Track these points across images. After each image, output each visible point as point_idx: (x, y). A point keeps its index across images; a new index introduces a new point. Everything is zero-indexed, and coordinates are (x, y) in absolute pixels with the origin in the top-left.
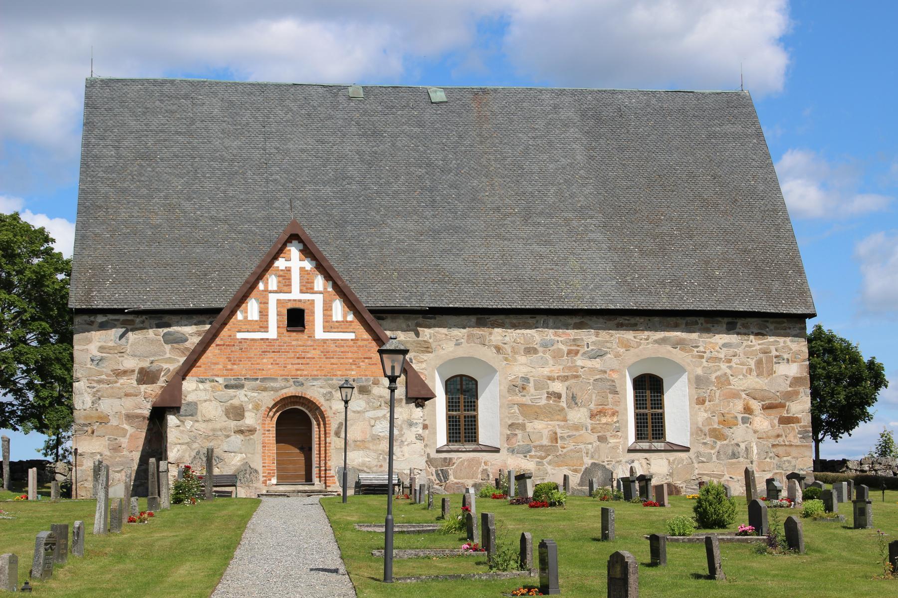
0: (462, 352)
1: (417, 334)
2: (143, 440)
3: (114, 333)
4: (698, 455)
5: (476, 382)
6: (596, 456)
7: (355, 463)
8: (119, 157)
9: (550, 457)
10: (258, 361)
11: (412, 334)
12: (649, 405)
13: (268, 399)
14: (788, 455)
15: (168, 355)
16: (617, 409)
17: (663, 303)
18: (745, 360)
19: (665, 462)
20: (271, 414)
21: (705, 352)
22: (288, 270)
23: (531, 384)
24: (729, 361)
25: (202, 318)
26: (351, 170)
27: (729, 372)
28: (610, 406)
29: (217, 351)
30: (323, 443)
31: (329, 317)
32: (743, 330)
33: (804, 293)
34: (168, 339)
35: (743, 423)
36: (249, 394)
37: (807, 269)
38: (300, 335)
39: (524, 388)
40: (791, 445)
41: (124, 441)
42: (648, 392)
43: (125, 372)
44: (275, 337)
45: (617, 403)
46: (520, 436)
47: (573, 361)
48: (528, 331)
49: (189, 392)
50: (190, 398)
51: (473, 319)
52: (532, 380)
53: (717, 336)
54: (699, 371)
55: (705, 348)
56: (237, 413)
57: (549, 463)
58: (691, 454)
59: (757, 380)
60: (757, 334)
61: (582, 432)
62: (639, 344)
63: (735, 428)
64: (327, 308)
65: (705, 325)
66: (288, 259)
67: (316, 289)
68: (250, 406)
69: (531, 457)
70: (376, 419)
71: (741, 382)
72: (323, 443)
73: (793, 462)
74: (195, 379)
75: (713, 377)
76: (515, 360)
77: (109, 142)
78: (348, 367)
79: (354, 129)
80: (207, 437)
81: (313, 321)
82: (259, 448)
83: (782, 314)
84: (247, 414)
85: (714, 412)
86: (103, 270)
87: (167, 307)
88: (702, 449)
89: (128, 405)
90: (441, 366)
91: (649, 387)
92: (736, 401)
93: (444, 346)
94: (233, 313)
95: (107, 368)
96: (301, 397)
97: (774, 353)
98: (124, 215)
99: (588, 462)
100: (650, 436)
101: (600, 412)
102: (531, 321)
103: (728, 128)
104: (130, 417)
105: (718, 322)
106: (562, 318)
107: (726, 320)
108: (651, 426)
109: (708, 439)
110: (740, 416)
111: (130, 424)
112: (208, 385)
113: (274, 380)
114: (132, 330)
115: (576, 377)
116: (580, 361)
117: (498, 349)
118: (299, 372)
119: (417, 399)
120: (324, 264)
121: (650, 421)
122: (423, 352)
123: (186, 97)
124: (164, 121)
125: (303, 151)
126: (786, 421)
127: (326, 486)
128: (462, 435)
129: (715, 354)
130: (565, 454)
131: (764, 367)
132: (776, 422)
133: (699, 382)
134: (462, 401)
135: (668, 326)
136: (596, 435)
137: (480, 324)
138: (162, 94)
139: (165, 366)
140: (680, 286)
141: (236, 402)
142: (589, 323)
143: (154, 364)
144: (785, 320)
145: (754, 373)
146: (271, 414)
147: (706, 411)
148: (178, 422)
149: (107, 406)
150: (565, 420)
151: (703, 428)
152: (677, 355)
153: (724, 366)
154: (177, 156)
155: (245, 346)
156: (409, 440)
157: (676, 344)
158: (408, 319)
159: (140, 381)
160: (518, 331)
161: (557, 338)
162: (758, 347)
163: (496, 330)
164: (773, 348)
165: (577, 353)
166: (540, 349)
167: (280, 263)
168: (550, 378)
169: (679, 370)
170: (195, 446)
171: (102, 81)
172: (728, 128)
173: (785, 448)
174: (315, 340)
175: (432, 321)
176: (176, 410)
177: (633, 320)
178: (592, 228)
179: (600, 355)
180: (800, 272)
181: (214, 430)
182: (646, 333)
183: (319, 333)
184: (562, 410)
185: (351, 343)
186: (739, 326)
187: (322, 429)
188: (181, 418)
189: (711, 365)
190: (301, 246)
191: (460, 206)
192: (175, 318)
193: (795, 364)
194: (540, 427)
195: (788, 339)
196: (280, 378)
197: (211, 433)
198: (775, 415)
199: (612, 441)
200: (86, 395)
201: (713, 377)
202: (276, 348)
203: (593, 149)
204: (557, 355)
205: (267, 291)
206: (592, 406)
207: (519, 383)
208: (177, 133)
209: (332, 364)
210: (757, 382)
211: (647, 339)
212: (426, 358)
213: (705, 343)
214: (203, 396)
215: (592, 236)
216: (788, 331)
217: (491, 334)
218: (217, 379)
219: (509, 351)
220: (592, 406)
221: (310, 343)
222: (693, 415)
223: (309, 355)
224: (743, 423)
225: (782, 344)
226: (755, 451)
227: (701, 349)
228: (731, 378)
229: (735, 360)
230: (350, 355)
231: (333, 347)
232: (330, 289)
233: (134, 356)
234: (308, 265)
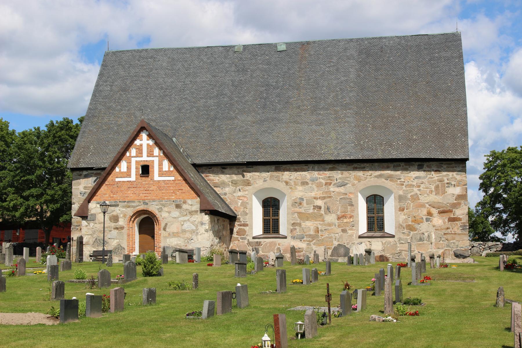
0: (267, 185)
1: (243, 176)
4: (400, 239)
5: (383, 198)
6: (341, 240)
7: (173, 244)
8: (111, 90)
9: (314, 241)
11: (241, 176)
16: (353, 214)
17: (379, 155)
18: (429, 186)
19: (380, 243)
20: (133, 219)
21: (404, 182)
22: (141, 145)
23: (305, 202)
24: (419, 186)
26: (226, 91)
27: (419, 193)
29: (106, 188)
31: (161, 168)
32: (427, 169)
33: (465, 146)
35: (427, 221)
36: (121, 209)
39: (300, 204)
40: (455, 234)
44: (134, 180)
45: (353, 211)
46: (298, 230)
48: (304, 173)
49: (92, 209)
51: (273, 167)
52: (305, 199)
53: (412, 173)
54: (401, 193)
55: (404, 179)
57: (314, 244)
58: (396, 239)
59: (436, 197)
60: (436, 171)
61: (333, 227)
62: (366, 178)
63: (421, 224)
64: (161, 164)
65: (405, 167)
66: (141, 140)
67: (155, 155)
68: (122, 215)
69: (304, 241)
70: (184, 221)
71: (426, 198)
73: (457, 243)
75: (409, 196)
76: (296, 189)
77: (108, 83)
79: (233, 68)
82: (126, 237)
83: (431, 158)
84: (120, 219)
85: (409, 215)
86: (88, 148)
88: (402, 236)
90: (256, 192)
91: (375, 202)
92: (422, 209)
93: (258, 182)
94: (113, 168)
97: (446, 181)
98: (106, 120)
99: (336, 243)
101: (343, 216)
102: (305, 167)
105: (412, 165)
106: (323, 165)
107: (417, 163)
108: (376, 223)
109: (405, 230)
110: (424, 218)
113: (133, 202)
115: (330, 197)
116: (332, 188)
117: (287, 183)
118: (146, 198)
119: (205, 210)
122: (246, 185)
123: (151, 57)
125: (203, 82)
126: (452, 220)
128: (271, 229)
129: (410, 183)
130: (323, 239)
131: (440, 189)
132: (447, 220)
133: (401, 199)
134: (271, 211)
135: (383, 168)
136: (340, 229)
137: (277, 170)
138: (140, 57)
141: (114, 213)
142: (337, 167)
144: (453, 162)
145: (434, 193)
146: (133, 219)
147: (404, 215)
148: (87, 224)
150: (323, 221)
151: (403, 224)
152: (388, 184)
153: (416, 190)
154: (139, 88)
155: (119, 185)
156: (201, 232)
157: (388, 178)
158: (238, 168)
160: (298, 173)
161: (319, 176)
162: (436, 178)
163: (286, 173)
164: (445, 179)
165: (330, 184)
166: (310, 182)
167: (137, 142)
168: (315, 198)
169: (390, 192)
170: (95, 236)
173: (452, 235)
174: (154, 181)
175: (251, 169)
177: (362, 165)
178: (349, 115)
179: (343, 185)
182: (370, 172)
183: (156, 177)
184: (322, 215)
185: (172, 182)
186: (425, 166)
189: (408, 189)
191: (279, 107)
193: (459, 188)
194: (309, 224)
195: (455, 173)
196: (136, 201)
198: (446, 217)
201: (409, 196)
202: (135, 185)
204: (319, 185)
205: (131, 157)
206: (339, 213)
207: (298, 201)
208: (143, 76)
209: (163, 193)
210: (436, 198)
211: (371, 176)
212: (247, 189)
213: (405, 177)
215: (348, 119)
216: (455, 168)
217: (283, 175)
219: (293, 184)
221: (151, 182)
222: (396, 217)
223: (151, 189)
224: (427, 221)
225: (451, 176)
226: (434, 237)
227: (403, 180)
228: (420, 196)
229: (422, 186)
230: (172, 188)
232: (162, 154)
234: (151, 142)
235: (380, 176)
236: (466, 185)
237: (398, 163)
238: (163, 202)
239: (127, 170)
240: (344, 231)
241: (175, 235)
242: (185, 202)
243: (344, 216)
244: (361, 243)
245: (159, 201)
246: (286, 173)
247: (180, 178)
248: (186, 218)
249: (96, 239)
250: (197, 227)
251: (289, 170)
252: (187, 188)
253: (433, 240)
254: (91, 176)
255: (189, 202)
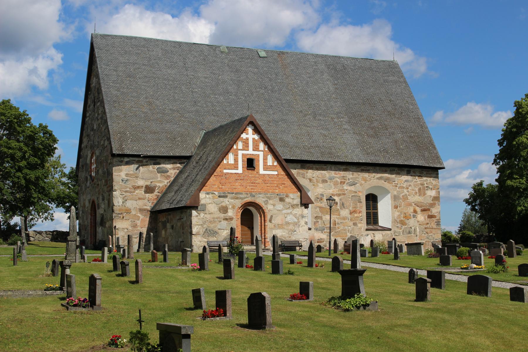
2: (148, 222)
3: (134, 167)
4: (395, 232)
10: (234, 184)
12: (371, 209)
13: (239, 203)
14: (431, 232)
15: (159, 179)
17: (382, 161)
18: (414, 188)
19: (381, 235)
22: (247, 139)
24: (408, 188)
25: (175, 161)
27: (407, 193)
28: (358, 209)
29: (215, 179)
30: (263, 225)
32: (413, 174)
33: (438, 158)
34: (160, 171)
36: (230, 200)
37: (437, 146)
38: (253, 172)
39: (321, 199)
41: (138, 223)
42: (371, 202)
43: (138, 187)
46: (320, 222)
47: (343, 187)
48: (323, 172)
49: (202, 199)
50: (202, 202)
51: (299, 165)
52: (325, 195)
53: (403, 177)
54: (395, 193)
56: (224, 210)
58: (392, 232)
60: (419, 176)
62: (371, 179)
64: (265, 159)
68: (230, 207)
69: (325, 232)
72: (263, 225)
74: (205, 192)
76: (318, 186)
78: (274, 188)
79: (227, 68)
80: (210, 222)
81: (259, 165)
84: (229, 210)
87: (160, 155)
89: (140, 203)
91: (372, 200)
92: (410, 207)
95: (130, 185)
96: (254, 203)
97: (426, 185)
100: (372, 223)
101: (354, 211)
102: (325, 167)
103: (391, 78)
104: (141, 210)
105: (403, 170)
106: (338, 166)
107: (406, 169)
108: (372, 218)
110: (412, 214)
111: (141, 214)
112: (211, 196)
113: (241, 194)
114: (142, 166)
115: (344, 194)
117: (310, 180)
118: (253, 190)
120: (265, 137)
121: (372, 216)
123: (144, 46)
124: (136, 58)
126: (431, 217)
127: (265, 247)
129: (402, 185)
131: (422, 192)
132: (426, 217)
133: (395, 198)
136: (352, 222)
137: (302, 168)
139: (158, 184)
140: (387, 152)
141: (224, 204)
143: (153, 183)
145: (418, 194)
147: (398, 212)
149: (130, 204)
150: (339, 215)
152: (386, 185)
153: (405, 191)
155: (227, 176)
157: (387, 180)
159: (146, 192)
161: (336, 176)
163: (309, 171)
164: (425, 183)
165: (344, 183)
166: (329, 181)
167: (244, 136)
170: (205, 226)
171: (100, 35)
172: (391, 78)
174: (260, 175)
176: (196, 208)
177: (368, 168)
180: (434, 148)
181: (214, 218)
182: (374, 174)
183: (262, 171)
187: (263, 218)
188: (199, 212)
190: (253, 127)
192: (162, 160)
196: (244, 193)
197: (212, 220)
198: (426, 214)
199: (359, 225)
200: (119, 198)
203: (336, 84)
204: (336, 184)
205: (237, 149)
206: (351, 208)
207: (320, 197)
208: (144, 65)
214: (208, 201)
215: (345, 127)
218: (215, 193)
220: (351, 208)
221: (257, 176)
227: (396, 182)
229: (410, 188)
230: (275, 182)
231: (268, 178)
232: (266, 149)
233: (143, 179)
234: (256, 137)
235: (380, 178)
236: (438, 189)
237: (393, 168)
238: (269, 195)
239: (234, 162)
240: (355, 224)
241: (280, 226)
242: (287, 196)
243: (355, 212)
244: (368, 235)
245: (265, 194)
246: (310, 171)
247: (283, 173)
248: (289, 211)
249: (206, 230)
250: (298, 220)
251: (312, 169)
252: (288, 182)
253: (418, 234)
254: (133, 163)
255: (291, 195)
